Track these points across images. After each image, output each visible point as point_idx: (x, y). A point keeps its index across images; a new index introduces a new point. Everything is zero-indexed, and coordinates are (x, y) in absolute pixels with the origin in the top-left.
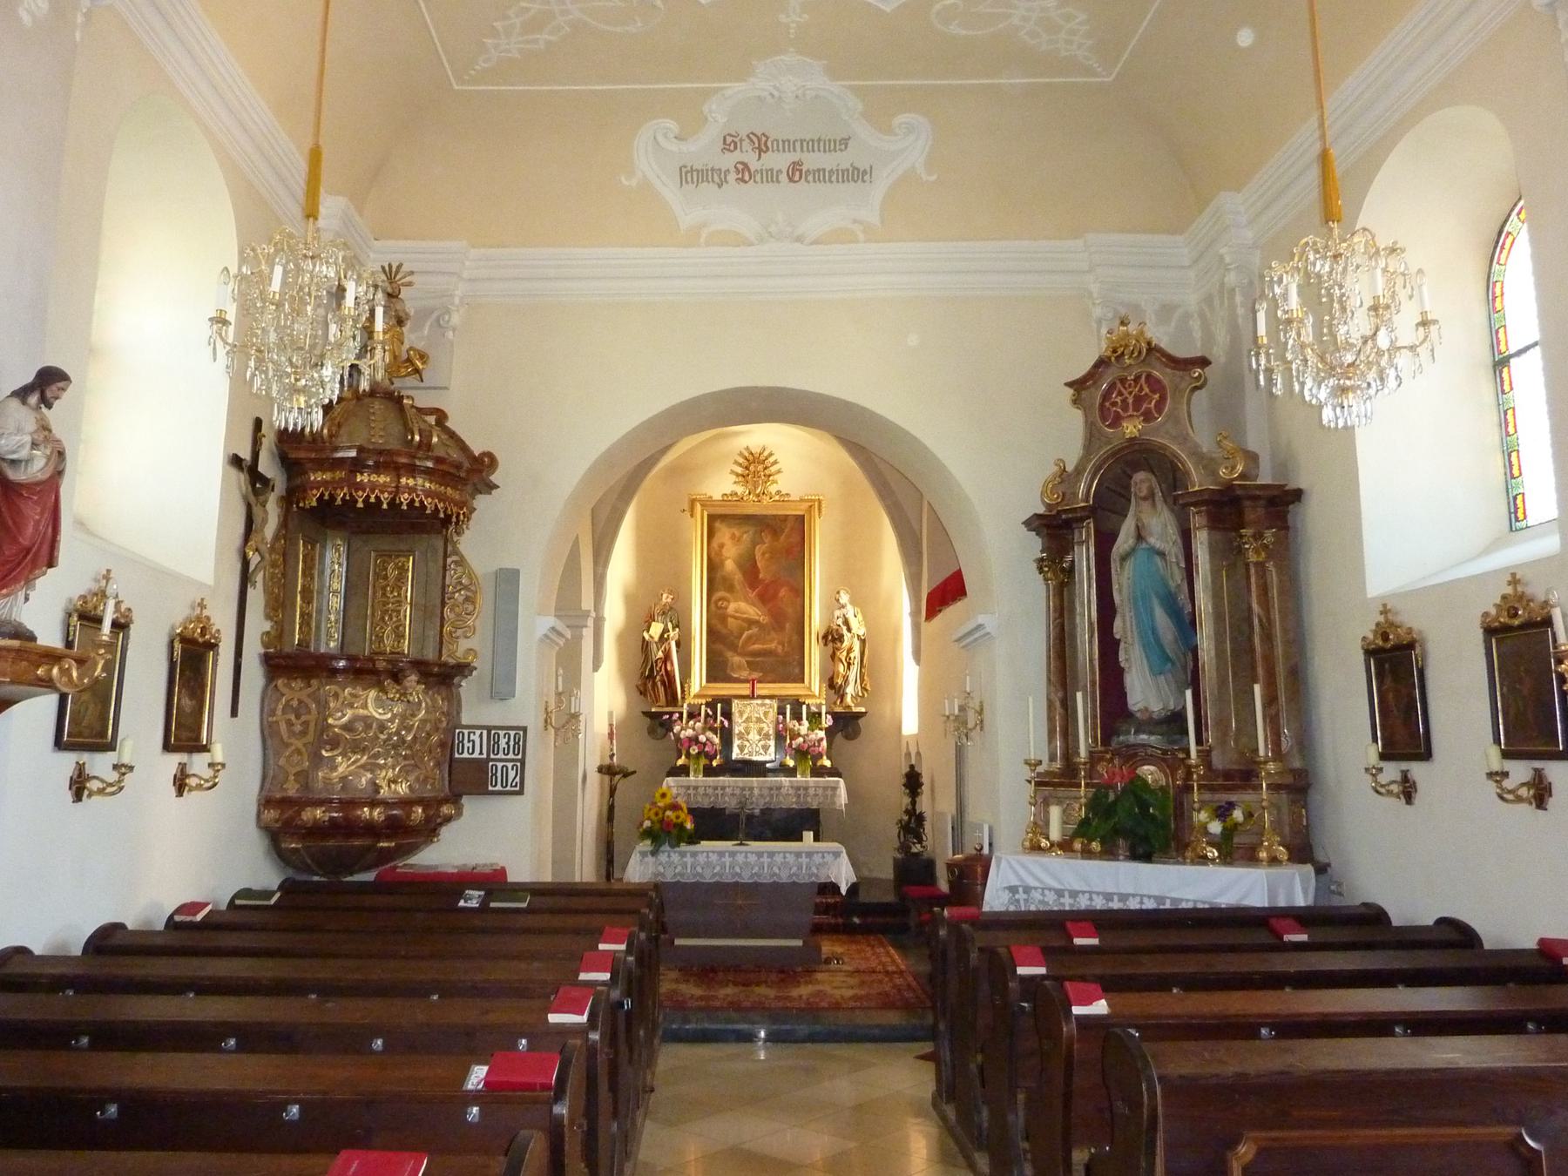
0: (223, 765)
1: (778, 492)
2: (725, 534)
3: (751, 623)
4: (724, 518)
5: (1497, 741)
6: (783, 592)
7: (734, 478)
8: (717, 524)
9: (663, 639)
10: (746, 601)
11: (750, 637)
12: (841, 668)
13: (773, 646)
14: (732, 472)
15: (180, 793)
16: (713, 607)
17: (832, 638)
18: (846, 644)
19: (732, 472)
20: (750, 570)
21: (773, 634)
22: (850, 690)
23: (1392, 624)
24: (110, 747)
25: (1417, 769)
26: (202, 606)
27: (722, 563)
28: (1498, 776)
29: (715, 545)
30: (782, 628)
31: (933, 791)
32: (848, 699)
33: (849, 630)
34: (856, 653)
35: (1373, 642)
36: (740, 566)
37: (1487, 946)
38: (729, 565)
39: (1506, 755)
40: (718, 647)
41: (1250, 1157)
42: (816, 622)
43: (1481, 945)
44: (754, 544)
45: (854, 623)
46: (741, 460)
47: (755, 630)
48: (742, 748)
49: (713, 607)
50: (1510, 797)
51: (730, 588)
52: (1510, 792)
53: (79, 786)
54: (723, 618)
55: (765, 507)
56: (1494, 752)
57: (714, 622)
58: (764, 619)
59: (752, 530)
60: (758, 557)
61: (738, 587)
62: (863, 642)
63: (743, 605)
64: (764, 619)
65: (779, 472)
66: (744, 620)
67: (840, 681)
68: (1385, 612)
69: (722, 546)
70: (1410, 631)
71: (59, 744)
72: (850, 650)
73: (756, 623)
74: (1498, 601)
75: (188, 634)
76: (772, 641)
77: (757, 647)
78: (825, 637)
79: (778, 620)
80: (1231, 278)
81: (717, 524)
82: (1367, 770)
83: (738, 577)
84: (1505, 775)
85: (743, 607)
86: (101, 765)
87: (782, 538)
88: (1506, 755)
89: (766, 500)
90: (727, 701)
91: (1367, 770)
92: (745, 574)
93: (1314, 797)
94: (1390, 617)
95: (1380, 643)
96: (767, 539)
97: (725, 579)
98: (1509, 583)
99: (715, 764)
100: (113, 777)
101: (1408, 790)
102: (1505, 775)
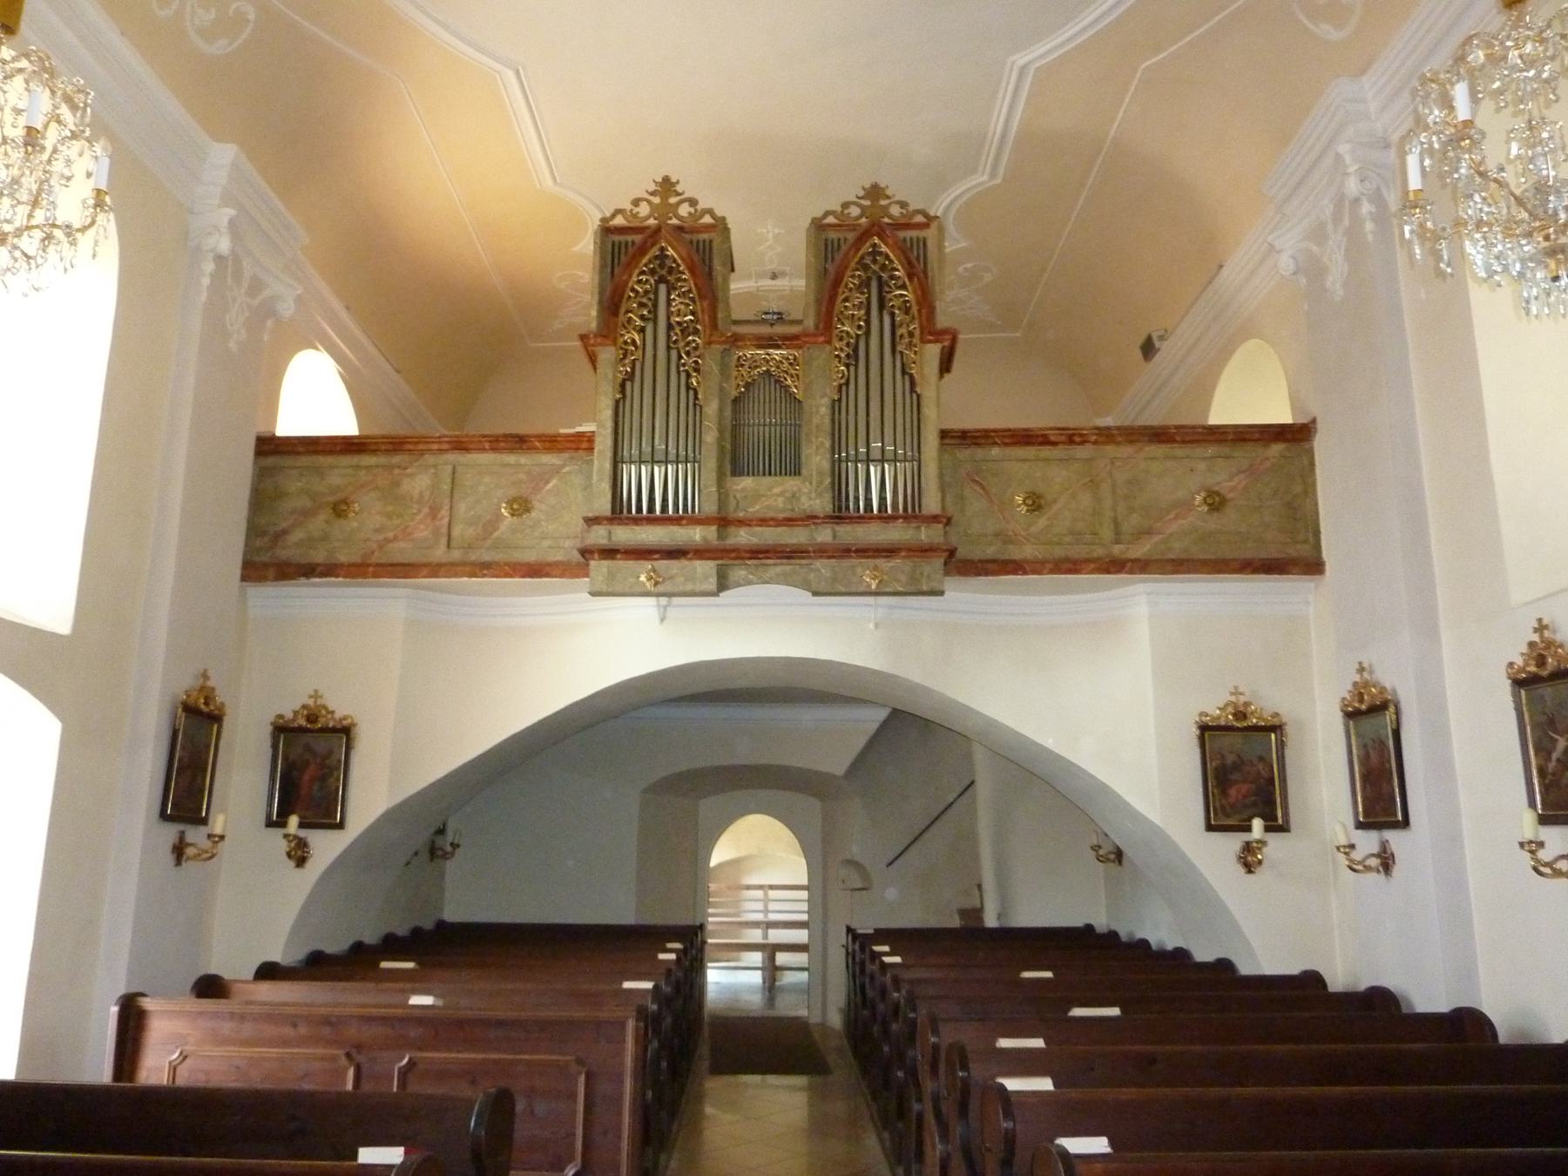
0: (222, 837)
5: (1532, 804)
15: (178, 862)
23: (1549, 644)
24: (204, 822)
25: (1393, 837)
26: (205, 676)
28: (1533, 846)
35: (1522, 670)
37: (1502, 1039)
39: (1544, 820)
41: (105, 149)
43: (1324, 985)
50: (1547, 870)
52: (1546, 865)
53: (179, 851)
56: (1528, 818)
68: (1541, 628)
70: (1383, 690)
71: (163, 816)
74: (1525, 649)
75: (191, 701)
80: (1352, 186)
82: (1522, 845)
84: (1541, 845)
86: (195, 835)
88: (1544, 820)
91: (1522, 845)
94: (1546, 634)
95: (1533, 669)
98: (1536, 630)
100: (207, 844)
101: (1386, 862)
102: (1541, 845)
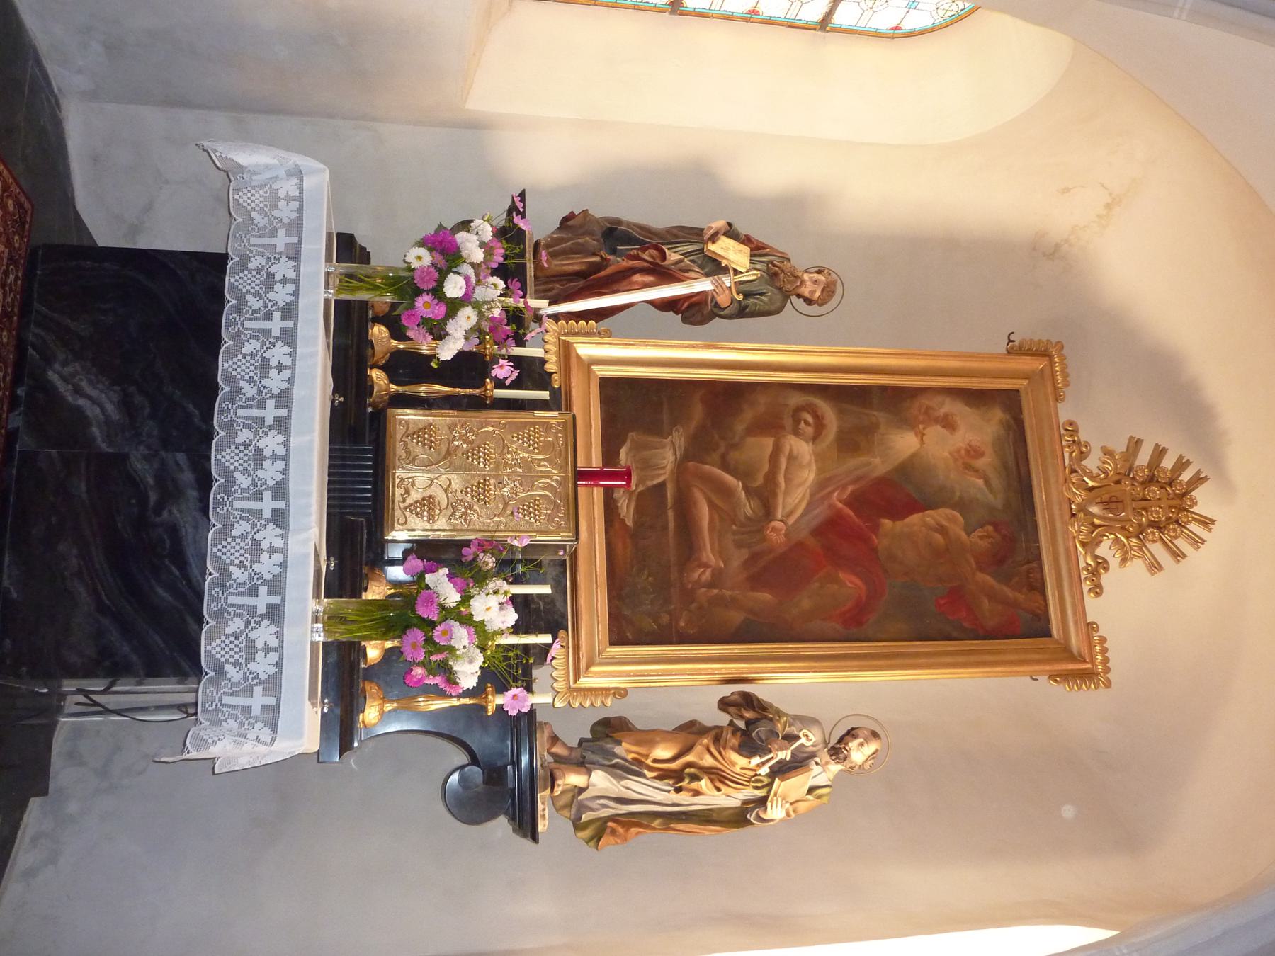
1: (1103, 564)
2: (978, 431)
3: (766, 497)
4: (1016, 431)
6: (850, 584)
7: (1120, 447)
8: (998, 414)
9: (715, 267)
10: (822, 485)
11: (726, 492)
12: (663, 752)
13: (708, 555)
14: (1135, 444)
16: (796, 399)
17: (752, 723)
18: (739, 762)
19: (1135, 444)
20: (897, 494)
21: (738, 558)
22: (600, 781)
27: (908, 423)
29: (950, 407)
30: (756, 580)
31: (673, 818)
32: (575, 779)
33: (782, 770)
34: (713, 797)
36: (907, 469)
38: (904, 443)
40: (698, 412)
42: (786, 683)
44: (962, 505)
45: (794, 786)
46: (1168, 463)
47: (748, 507)
48: (421, 433)
49: (796, 399)
51: (850, 442)
54: (770, 425)
55: (1060, 537)
57: (763, 400)
58: (777, 532)
59: (997, 501)
60: (932, 516)
61: (853, 462)
62: (739, 818)
63: (808, 476)
64: (777, 532)
65: (1155, 567)
66: (771, 477)
67: (626, 750)
69: (948, 423)
72: (718, 777)
73: (768, 511)
76: (721, 553)
77: (704, 512)
78: (749, 701)
79: (778, 569)
81: (998, 414)
83: (878, 465)
85: (804, 479)
87: (985, 578)
89: (1078, 529)
90: (558, 401)
92: (883, 482)
93: (634, 212)
96: (980, 540)
97: (869, 430)
99: (375, 374)
